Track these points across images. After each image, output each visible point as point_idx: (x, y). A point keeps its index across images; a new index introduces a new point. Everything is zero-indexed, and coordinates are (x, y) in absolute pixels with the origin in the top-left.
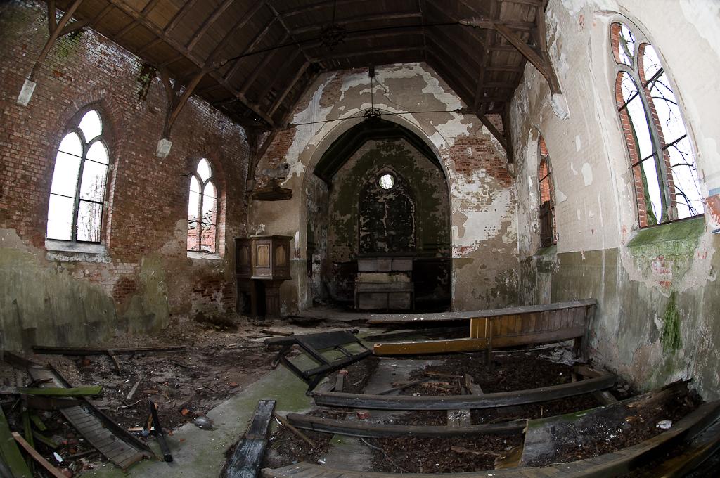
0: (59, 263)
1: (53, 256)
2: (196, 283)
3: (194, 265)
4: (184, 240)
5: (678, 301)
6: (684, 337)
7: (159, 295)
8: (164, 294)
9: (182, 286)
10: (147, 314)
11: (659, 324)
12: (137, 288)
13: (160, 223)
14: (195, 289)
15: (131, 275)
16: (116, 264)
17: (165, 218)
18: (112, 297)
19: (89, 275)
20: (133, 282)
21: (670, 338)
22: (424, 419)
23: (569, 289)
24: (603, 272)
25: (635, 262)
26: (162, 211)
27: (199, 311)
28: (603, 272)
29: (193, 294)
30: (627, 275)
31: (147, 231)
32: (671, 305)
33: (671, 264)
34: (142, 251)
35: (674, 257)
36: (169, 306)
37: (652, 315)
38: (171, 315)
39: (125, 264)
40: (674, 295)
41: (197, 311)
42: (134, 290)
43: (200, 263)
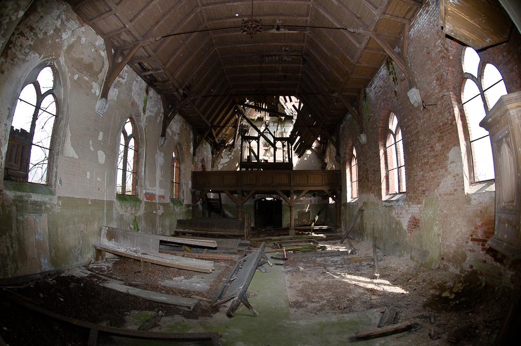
0: (386, 206)
1: (384, 203)
2: (477, 228)
3: (473, 202)
4: (458, 172)
5: (137, 219)
6: (140, 228)
7: (434, 235)
8: (439, 235)
9: (458, 230)
10: (424, 250)
11: (132, 227)
12: (421, 226)
13: (434, 163)
14: (474, 237)
15: (418, 214)
16: (409, 206)
17: (438, 156)
18: (406, 229)
19: (397, 214)
20: (418, 220)
21: (136, 229)
22: (214, 235)
23: (74, 224)
24: (105, 212)
25: (122, 207)
26: (434, 150)
27: (474, 268)
28: (105, 212)
29: (471, 243)
30: (118, 213)
31: (425, 175)
32: (135, 220)
33: (134, 208)
34: (424, 194)
35: (135, 206)
36: (442, 249)
37: (129, 225)
38: (443, 259)
39: (414, 206)
40: (136, 217)
41: (471, 267)
42: (419, 227)
43: (481, 199)
